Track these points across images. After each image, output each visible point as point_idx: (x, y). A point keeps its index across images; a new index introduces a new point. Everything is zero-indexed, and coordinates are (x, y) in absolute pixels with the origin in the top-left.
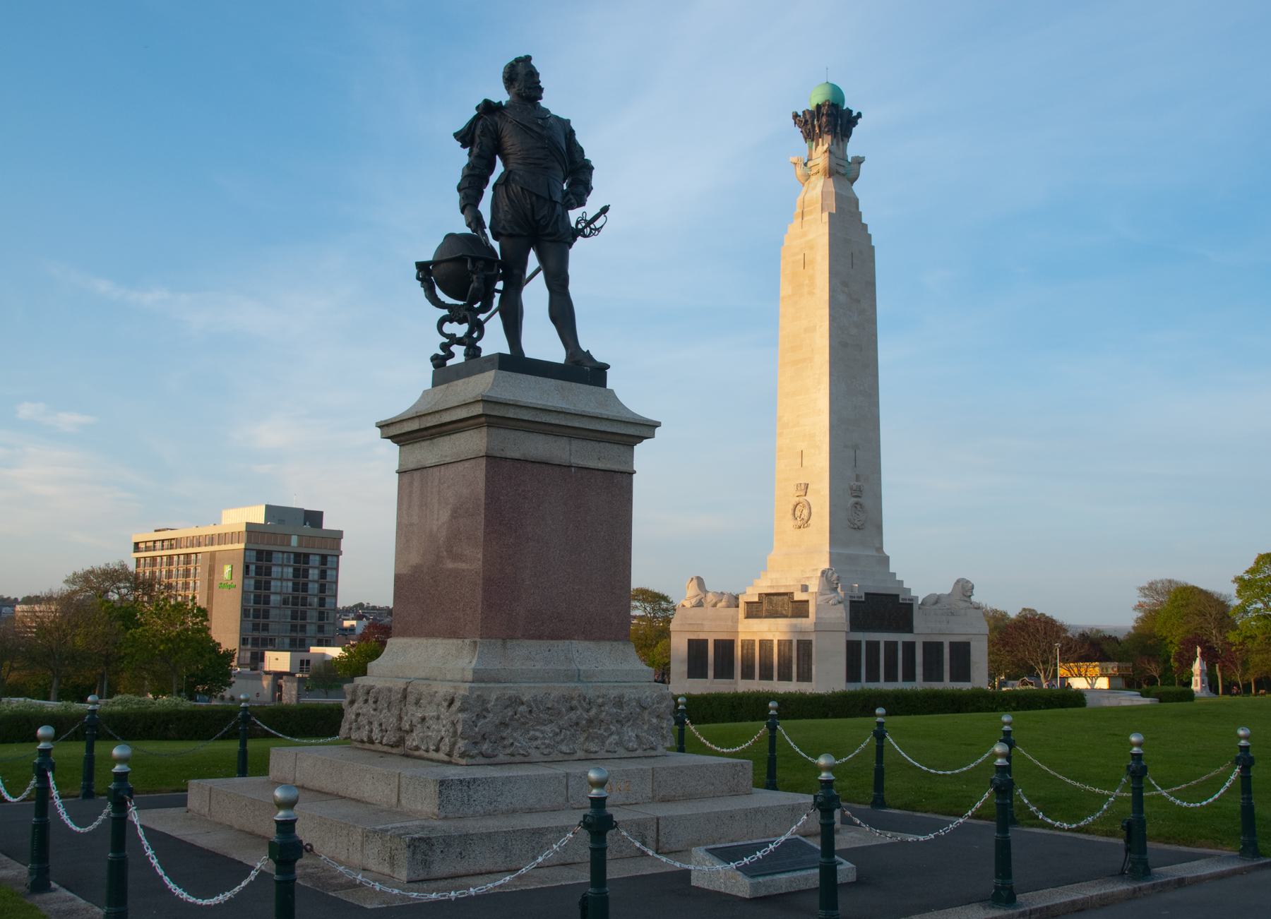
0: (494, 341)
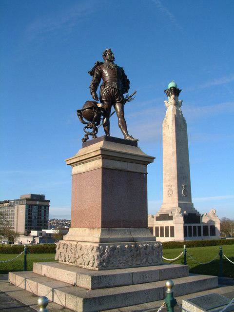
0: (101, 132)
